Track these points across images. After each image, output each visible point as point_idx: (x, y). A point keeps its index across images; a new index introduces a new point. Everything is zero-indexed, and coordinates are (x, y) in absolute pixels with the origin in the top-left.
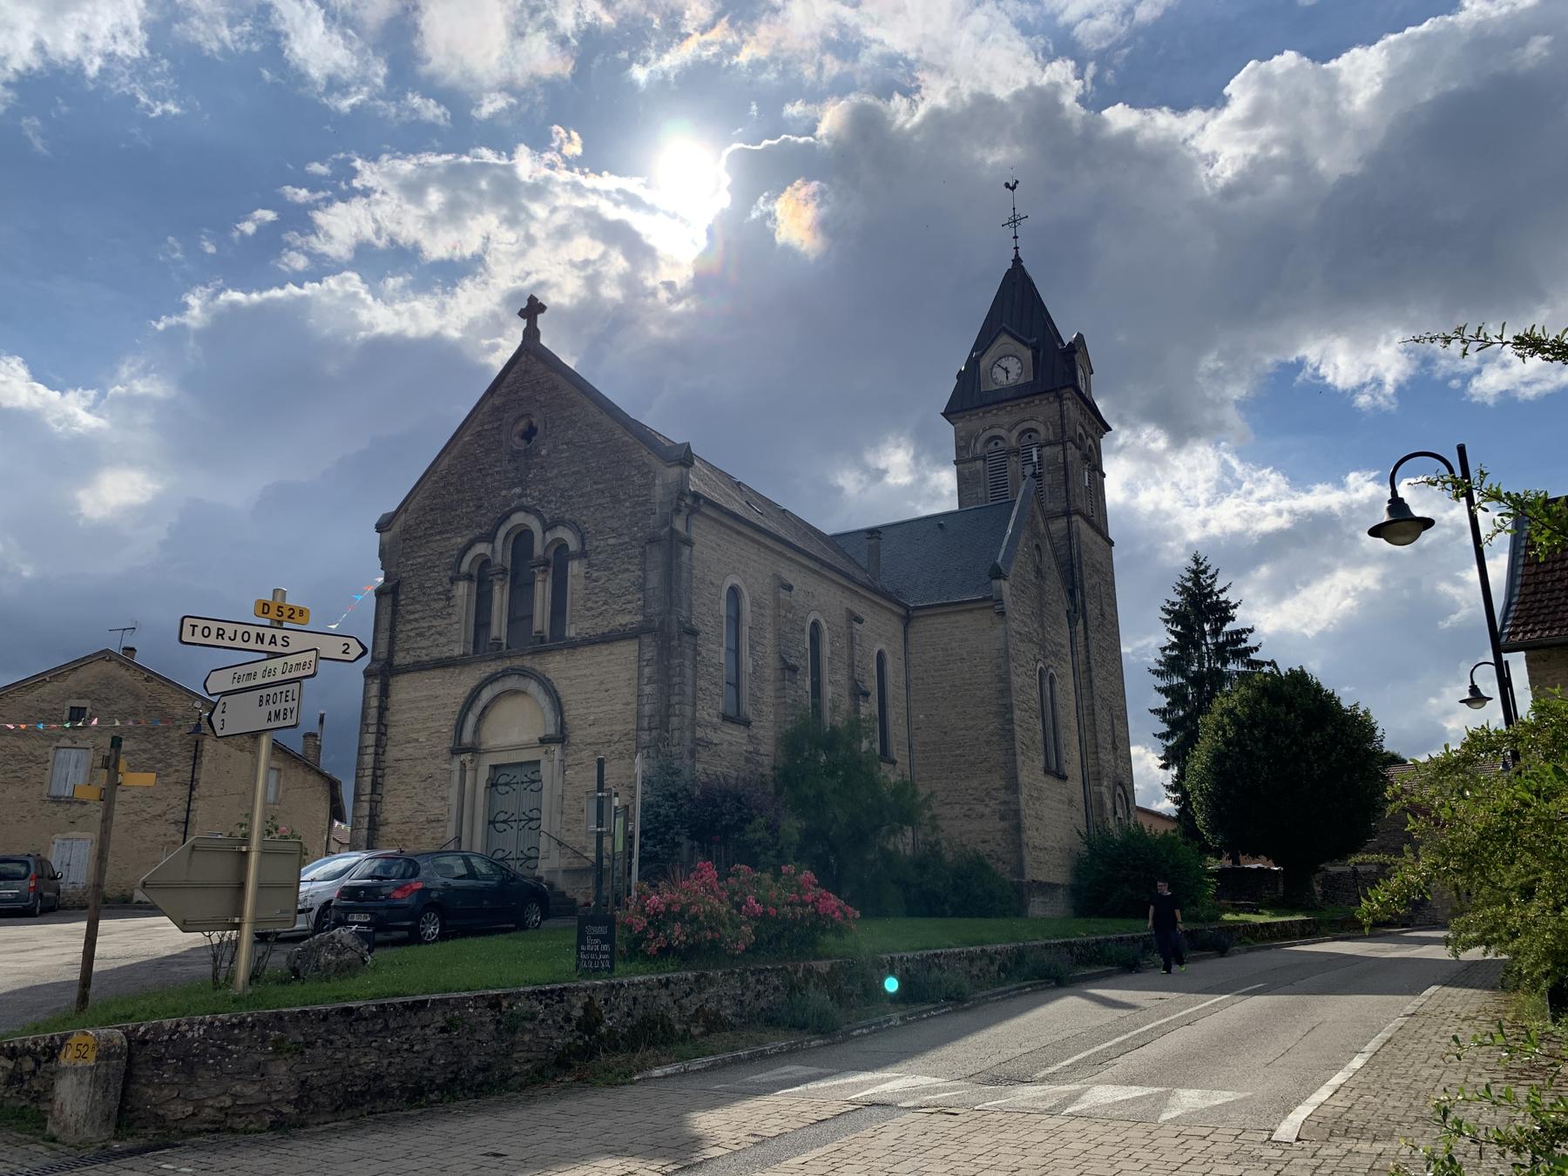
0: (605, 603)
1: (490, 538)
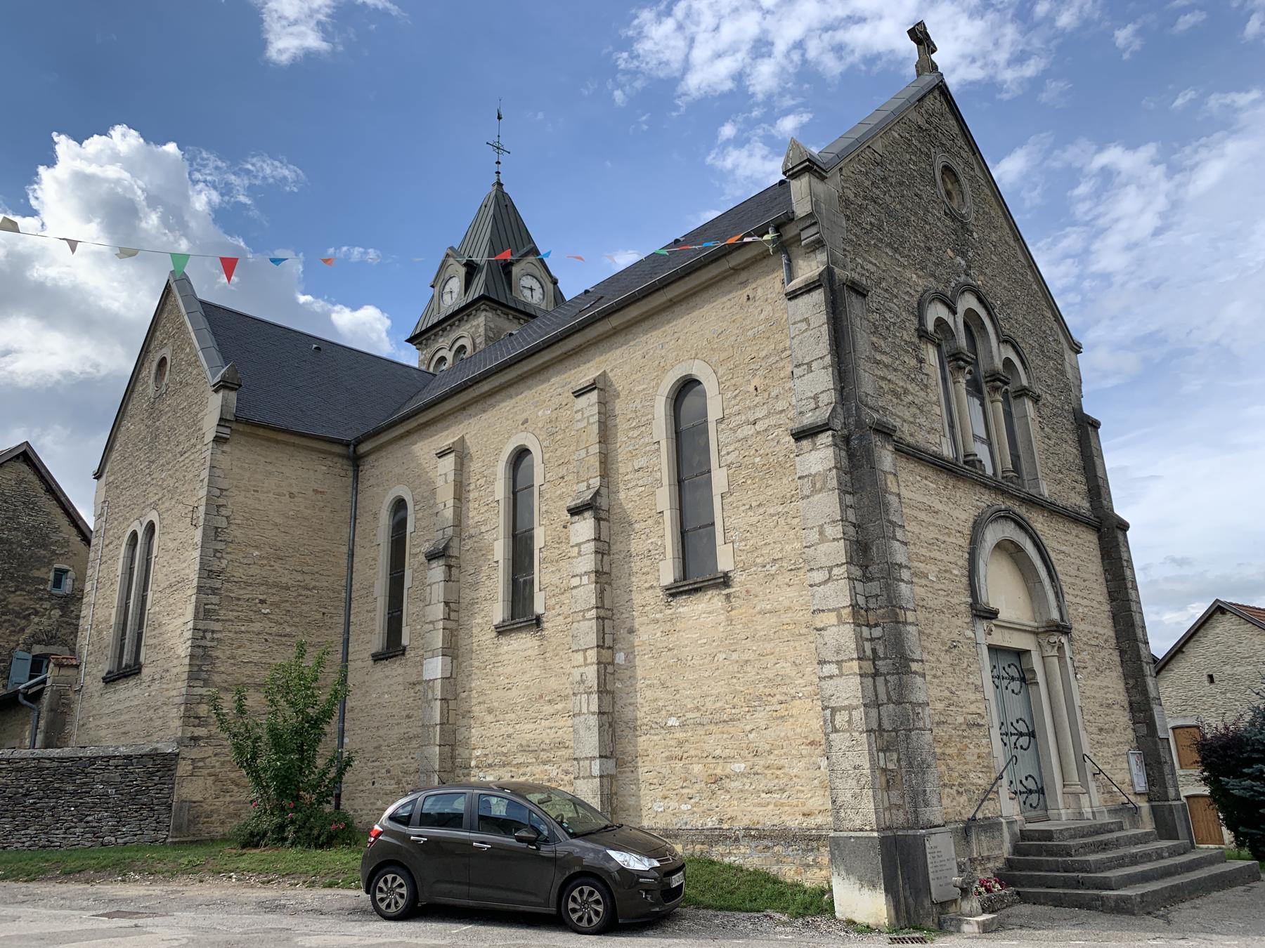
0: (1060, 471)
1: (1006, 340)
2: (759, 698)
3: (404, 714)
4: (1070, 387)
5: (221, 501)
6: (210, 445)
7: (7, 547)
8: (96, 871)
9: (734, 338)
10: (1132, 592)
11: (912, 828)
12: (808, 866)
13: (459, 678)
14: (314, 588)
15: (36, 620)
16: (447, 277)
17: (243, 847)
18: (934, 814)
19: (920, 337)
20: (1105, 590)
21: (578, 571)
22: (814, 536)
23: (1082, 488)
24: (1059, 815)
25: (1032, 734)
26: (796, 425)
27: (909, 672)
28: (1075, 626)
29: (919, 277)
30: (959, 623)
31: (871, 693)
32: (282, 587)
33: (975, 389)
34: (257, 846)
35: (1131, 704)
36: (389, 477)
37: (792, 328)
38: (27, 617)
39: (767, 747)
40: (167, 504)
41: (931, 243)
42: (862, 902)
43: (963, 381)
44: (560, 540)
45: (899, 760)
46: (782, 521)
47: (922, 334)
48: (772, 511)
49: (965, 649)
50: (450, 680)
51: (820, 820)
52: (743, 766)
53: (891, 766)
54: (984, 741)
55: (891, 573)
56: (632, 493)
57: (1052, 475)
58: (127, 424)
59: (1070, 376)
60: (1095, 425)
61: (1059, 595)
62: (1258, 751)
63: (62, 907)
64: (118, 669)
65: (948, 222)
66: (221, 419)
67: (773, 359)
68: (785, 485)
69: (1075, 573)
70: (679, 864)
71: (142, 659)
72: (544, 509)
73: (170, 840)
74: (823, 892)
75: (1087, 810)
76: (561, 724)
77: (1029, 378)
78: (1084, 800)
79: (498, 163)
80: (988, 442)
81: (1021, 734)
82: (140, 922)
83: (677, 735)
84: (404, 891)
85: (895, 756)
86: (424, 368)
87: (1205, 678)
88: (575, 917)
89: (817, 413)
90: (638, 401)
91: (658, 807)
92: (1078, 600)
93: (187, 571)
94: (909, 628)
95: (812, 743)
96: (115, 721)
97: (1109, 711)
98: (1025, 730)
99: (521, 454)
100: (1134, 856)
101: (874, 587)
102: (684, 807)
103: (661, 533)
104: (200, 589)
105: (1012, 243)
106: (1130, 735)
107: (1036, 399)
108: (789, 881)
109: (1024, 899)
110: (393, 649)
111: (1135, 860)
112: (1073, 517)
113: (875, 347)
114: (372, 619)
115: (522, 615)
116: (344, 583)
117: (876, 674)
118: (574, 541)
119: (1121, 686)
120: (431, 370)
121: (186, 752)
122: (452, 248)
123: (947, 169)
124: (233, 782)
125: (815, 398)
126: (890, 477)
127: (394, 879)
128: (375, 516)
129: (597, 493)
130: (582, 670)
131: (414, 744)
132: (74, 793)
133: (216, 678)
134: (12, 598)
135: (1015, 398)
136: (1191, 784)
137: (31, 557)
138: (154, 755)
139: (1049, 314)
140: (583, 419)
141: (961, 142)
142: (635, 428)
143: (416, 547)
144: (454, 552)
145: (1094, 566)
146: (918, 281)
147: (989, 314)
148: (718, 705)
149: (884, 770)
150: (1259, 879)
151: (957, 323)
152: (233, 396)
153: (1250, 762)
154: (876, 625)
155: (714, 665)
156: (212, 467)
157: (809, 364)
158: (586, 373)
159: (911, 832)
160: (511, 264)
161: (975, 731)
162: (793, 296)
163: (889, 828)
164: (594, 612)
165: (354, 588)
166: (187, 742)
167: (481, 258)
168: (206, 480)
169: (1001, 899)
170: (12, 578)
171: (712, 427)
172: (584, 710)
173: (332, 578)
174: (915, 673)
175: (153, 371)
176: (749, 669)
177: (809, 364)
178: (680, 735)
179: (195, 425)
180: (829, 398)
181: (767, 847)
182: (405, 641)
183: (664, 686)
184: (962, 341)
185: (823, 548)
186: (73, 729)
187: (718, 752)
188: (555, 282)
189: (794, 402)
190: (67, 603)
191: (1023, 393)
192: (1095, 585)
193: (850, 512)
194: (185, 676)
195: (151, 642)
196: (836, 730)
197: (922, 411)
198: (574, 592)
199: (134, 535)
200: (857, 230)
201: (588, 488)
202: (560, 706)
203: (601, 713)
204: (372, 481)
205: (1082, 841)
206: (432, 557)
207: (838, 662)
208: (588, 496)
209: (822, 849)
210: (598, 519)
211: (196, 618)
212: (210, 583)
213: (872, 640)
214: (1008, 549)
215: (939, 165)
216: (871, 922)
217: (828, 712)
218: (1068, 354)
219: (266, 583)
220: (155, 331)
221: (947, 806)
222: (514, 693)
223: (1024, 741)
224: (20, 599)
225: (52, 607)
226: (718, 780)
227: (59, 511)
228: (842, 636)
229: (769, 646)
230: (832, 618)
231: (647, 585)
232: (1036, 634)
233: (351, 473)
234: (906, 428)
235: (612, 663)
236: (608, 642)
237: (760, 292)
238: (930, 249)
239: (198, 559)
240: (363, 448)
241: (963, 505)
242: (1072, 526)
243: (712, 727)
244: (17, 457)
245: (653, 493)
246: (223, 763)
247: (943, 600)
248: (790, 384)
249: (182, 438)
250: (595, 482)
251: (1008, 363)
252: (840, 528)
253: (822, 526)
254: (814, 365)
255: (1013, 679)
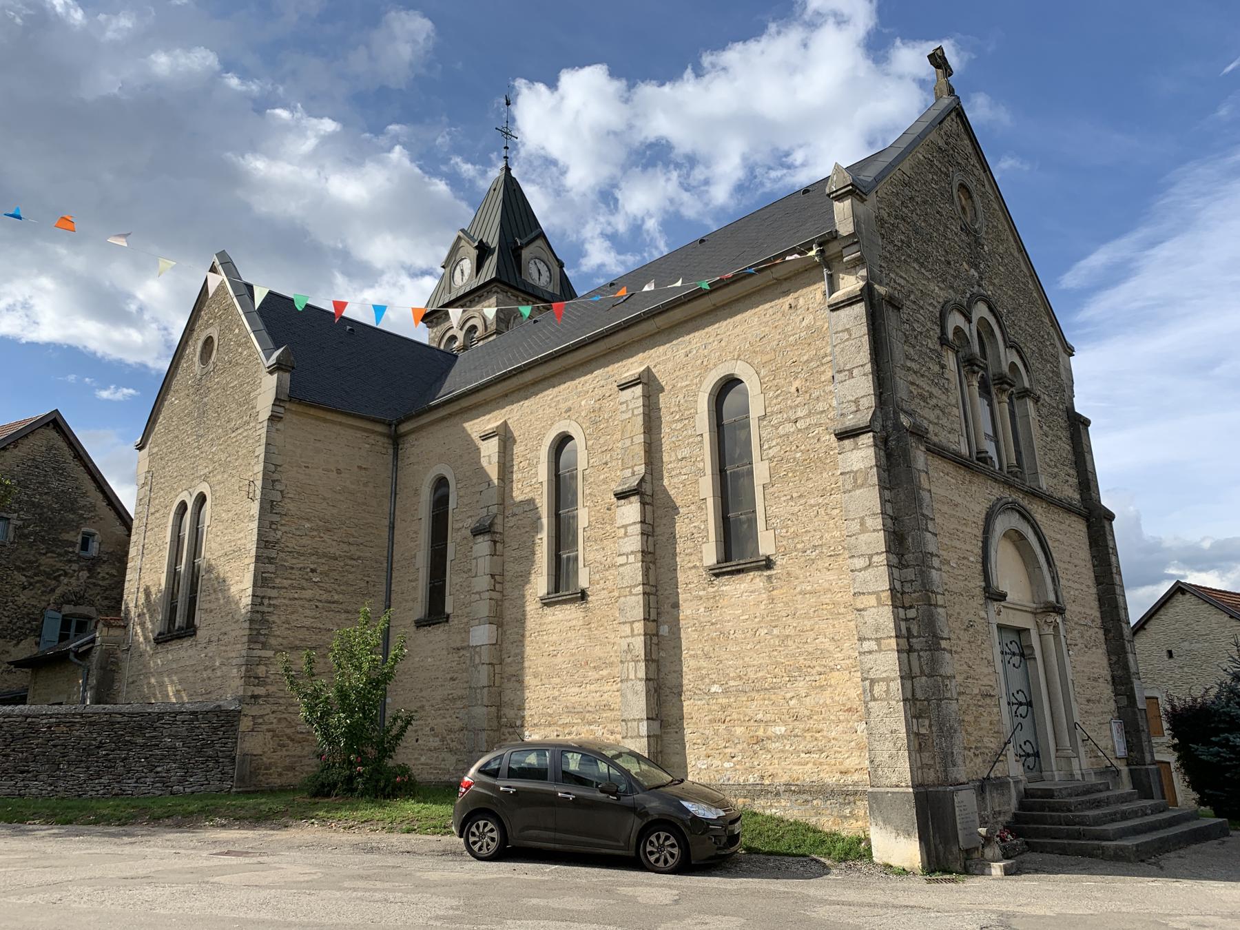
1: (1011, 345)
2: (800, 669)
3: (449, 676)
4: (1064, 386)
5: (276, 476)
6: (265, 424)
7: (38, 511)
8: (183, 816)
9: (775, 343)
10: (1116, 577)
11: (941, 785)
12: (846, 817)
13: (504, 645)
14: (359, 558)
15: (66, 581)
16: (458, 258)
17: (315, 795)
18: (961, 772)
19: (942, 345)
20: (1092, 575)
21: (625, 550)
22: (855, 526)
23: (1074, 481)
24: (1053, 776)
25: (1029, 704)
26: (839, 427)
27: (940, 649)
28: (1068, 607)
29: (941, 288)
30: (975, 604)
31: (906, 668)
32: (331, 558)
33: (985, 390)
34: (328, 795)
35: (1113, 677)
36: (428, 454)
37: (834, 337)
38: (56, 578)
39: (807, 713)
40: (219, 477)
41: (950, 258)
42: (899, 848)
43: (976, 384)
44: (606, 518)
45: (930, 726)
46: (822, 511)
47: (943, 341)
48: (812, 502)
49: (979, 628)
50: (498, 645)
51: (856, 777)
52: (783, 729)
53: (923, 731)
54: (996, 710)
55: (924, 561)
56: (676, 480)
57: (1049, 470)
58: (172, 399)
59: (1063, 377)
60: (1086, 423)
61: (1055, 579)
62: (1225, 722)
63: (434, 834)
64: (169, 631)
65: (964, 237)
66: (276, 399)
67: (813, 364)
68: (825, 479)
69: (1069, 559)
70: (737, 815)
71: (197, 622)
72: (587, 492)
73: (234, 789)
74: (860, 841)
75: (1077, 772)
76: (606, 688)
77: (1030, 380)
78: (1075, 762)
79: (506, 148)
80: (995, 438)
81: (1021, 704)
82: (265, 859)
83: (720, 701)
84: (495, 835)
85: (927, 722)
86: (434, 345)
87: (1165, 654)
88: (652, 859)
89: (859, 415)
90: (681, 396)
91: (702, 764)
92: (1071, 583)
93: (243, 541)
94: (940, 610)
95: (849, 710)
96: (169, 682)
97: (1095, 684)
98: (1024, 701)
99: (564, 440)
100: (1124, 812)
101: (910, 573)
102: (727, 765)
103: (704, 518)
104: (258, 558)
105: (1016, 254)
106: (1112, 705)
107: (1037, 400)
108: (827, 830)
109: (1032, 848)
110: (435, 614)
111: (1125, 816)
112: (1067, 508)
113: (907, 357)
114: (415, 588)
115: (564, 587)
116: (385, 553)
117: (910, 650)
118: (619, 522)
119: (1105, 662)
120: (442, 347)
121: (247, 710)
122: (463, 230)
123: (963, 186)
124: (289, 738)
125: (856, 401)
126: (923, 475)
127: (485, 825)
128: (416, 492)
129: (642, 480)
130: (629, 640)
131: (459, 704)
132: (144, 746)
133: (273, 641)
134: (43, 560)
135: (1018, 398)
136: (1163, 750)
137: (61, 521)
138: (219, 711)
139: (1047, 320)
140: (628, 410)
141: (974, 161)
142: (678, 421)
143: (460, 522)
144: (498, 528)
145: (1083, 554)
146: (939, 293)
147: (998, 322)
148: (760, 674)
149: (917, 734)
150: (1228, 835)
151: (971, 330)
152: (287, 376)
153: (1217, 732)
154: (911, 607)
155: (756, 639)
156: (267, 444)
157: (851, 371)
158: (632, 367)
159: (940, 789)
160: (521, 248)
161: (988, 701)
162: (835, 307)
163: (921, 785)
164: (640, 588)
165: (395, 558)
166: (247, 700)
167: (493, 242)
168: (262, 456)
169: (1014, 847)
170: (43, 541)
171: (754, 424)
172: (632, 676)
173: (374, 550)
174: (944, 649)
175: (199, 350)
176: (790, 643)
177: (851, 371)
178: (724, 701)
179: (247, 403)
180: (869, 402)
181: (807, 801)
182: (448, 609)
183: (707, 656)
184: (976, 348)
185: (863, 538)
186: (122, 687)
187: (760, 716)
188: (561, 265)
189: (834, 403)
190: (94, 565)
191: (1025, 393)
192: (1084, 570)
193: (888, 505)
194: (245, 639)
195: (205, 606)
196: (874, 699)
197: (944, 413)
198: (621, 569)
199: (183, 506)
200: (890, 247)
201: (633, 474)
202: (604, 673)
203: (647, 679)
204: (412, 459)
205: (1080, 799)
206: (477, 532)
207: (876, 639)
208: (634, 482)
209: (858, 803)
210: (643, 504)
211: (255, 585)
212: (267, 553)
213: (906, 620)
214: (1016, 538)
215: (956, 185)
216: (907, 865)
217: (867, 683)
218: (1063, 355)
219: (316, 554)
220: (200, 310)
221: (967, 768)
222: (559, 659)
223: (1023, 710)
224: (51, 561)
225: (81, 569)
226: (759, 741)
227: (87, 477)
228: (882, 617)
229: (808, 624)
230: (872, 600)
231: (690, 565)
232: (1034, 614)
233: (391, 451)
234: (931, 428)
235: (657, 635)
236: (653, 616)
237: (801, 301)
238: (949, 263)
239: (256, 531)
240: (404, 428)
241: (975, 498)
242: (1066, 515)
243: (754, 694)
244: (47, 424)
245: (697, 482)
246: (280, 720)
247: (961, 584)
248: (831, 388)
249: (233, 415)
250: (641, 469)
251: (1013, 366)
252: (880, 520)
253: (862, 518)
254: (855, 372)
255: (1014, 654)
